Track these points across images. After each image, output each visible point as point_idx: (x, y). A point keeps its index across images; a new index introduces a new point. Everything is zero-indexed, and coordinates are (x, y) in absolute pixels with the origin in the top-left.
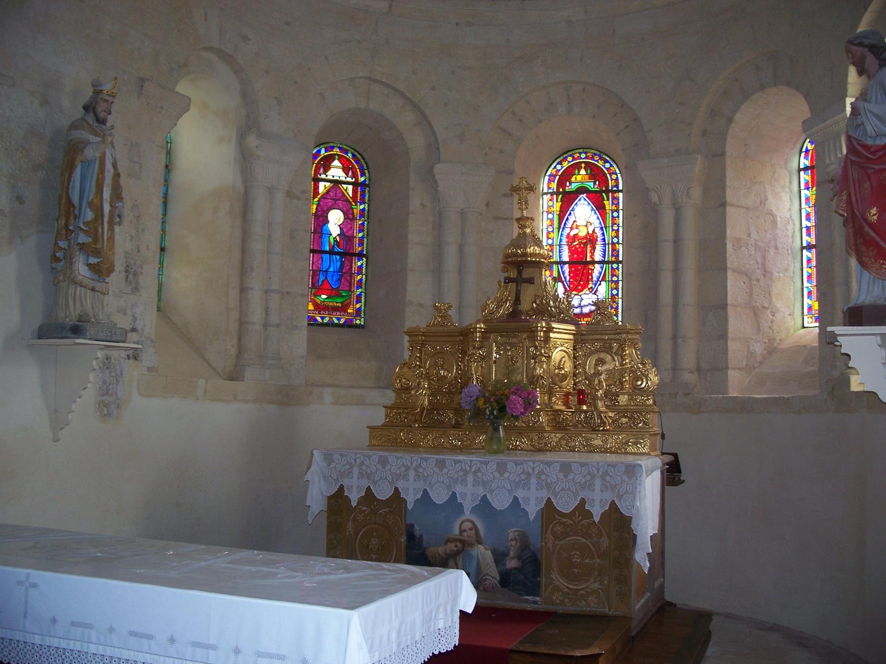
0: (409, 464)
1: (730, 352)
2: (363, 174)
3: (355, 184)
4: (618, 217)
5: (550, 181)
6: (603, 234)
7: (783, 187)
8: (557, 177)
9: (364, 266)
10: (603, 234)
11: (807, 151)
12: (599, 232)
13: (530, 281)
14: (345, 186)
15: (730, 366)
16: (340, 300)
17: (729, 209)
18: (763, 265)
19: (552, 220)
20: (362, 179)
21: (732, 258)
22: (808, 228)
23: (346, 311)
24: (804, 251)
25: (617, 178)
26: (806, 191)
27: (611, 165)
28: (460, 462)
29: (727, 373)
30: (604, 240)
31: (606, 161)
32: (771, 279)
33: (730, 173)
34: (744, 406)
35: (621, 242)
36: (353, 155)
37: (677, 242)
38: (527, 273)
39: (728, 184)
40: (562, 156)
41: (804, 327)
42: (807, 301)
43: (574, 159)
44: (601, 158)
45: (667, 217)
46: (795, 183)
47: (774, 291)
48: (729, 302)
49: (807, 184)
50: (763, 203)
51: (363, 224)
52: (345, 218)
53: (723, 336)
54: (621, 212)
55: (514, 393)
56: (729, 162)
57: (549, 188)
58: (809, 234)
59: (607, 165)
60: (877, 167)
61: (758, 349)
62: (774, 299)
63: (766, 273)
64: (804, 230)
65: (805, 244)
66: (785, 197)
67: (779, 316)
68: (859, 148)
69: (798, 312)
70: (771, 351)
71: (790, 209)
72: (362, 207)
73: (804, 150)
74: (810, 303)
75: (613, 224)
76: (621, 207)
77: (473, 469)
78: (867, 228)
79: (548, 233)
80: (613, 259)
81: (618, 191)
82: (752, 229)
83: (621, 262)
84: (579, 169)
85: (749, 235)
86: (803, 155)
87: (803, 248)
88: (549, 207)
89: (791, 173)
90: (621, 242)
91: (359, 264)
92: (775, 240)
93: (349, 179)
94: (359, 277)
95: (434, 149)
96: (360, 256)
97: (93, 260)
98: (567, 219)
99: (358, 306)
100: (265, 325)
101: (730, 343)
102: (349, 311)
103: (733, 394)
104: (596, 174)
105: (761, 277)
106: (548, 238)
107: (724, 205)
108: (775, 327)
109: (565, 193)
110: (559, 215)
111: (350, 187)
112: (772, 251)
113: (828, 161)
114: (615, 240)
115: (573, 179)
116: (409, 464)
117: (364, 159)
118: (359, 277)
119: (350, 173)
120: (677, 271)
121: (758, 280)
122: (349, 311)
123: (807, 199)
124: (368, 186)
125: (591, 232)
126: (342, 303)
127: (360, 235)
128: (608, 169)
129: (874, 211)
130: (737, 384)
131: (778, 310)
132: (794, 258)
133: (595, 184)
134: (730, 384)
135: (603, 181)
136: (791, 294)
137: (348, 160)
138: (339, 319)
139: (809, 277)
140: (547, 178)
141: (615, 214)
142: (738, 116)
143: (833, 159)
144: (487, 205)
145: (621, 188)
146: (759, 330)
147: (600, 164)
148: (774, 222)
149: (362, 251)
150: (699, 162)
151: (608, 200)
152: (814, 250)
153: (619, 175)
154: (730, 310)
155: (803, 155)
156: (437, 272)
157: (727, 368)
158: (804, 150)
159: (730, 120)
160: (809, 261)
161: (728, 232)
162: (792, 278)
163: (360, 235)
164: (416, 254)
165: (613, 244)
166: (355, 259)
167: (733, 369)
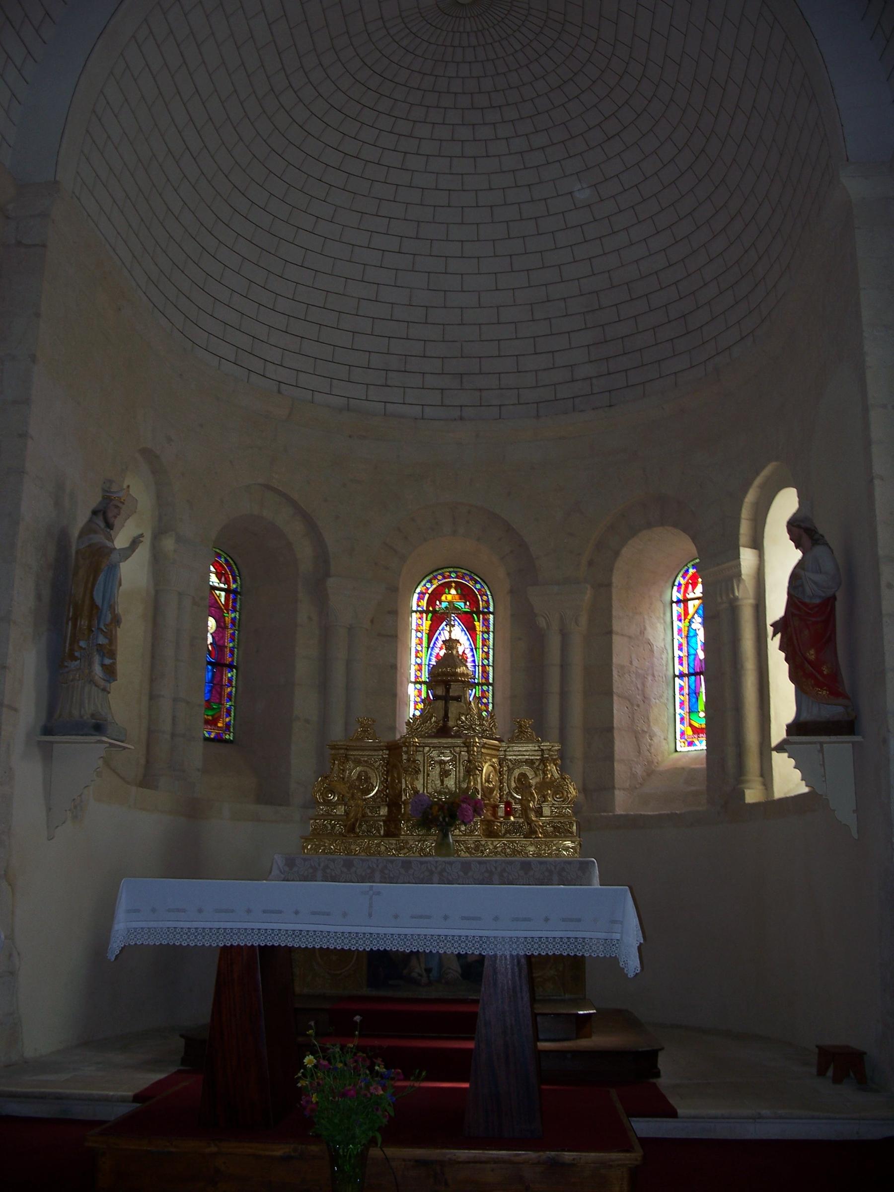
0: (375, 866)
1: (616, 773)
2: (235, 581)
3: (227, 591)
4: (488, 639)
5: (419, 599)
6: (473, 656)
7: (658, 618)
8: (427, 596)
9: (234, 678)
10: (473, 656)
11: (680, 585)
12: (469, 655)
13: (458, 699)
14: (217, 592)
15: (616, 786)
16: (210, 713)
17: (615, 637)
18: (643, 691)
19: (421, 639)
20: (234, 586)
21: (618, 684)
22: (680, 658)
23: (216, 724)
24: (676, 679)
25: (487, 600)
26: (679, 623)
27: (482, 586)
28: (426, 862)
29: (613, 793)
30: (474, 661)
31: (477, 582)
32: (649, 705)
33: (615, 604)
34: (632, 822)
35: (491, 664)
36: (226, 560)
37: (564, 666)
38: (454, 691)
39: (614, 613)
40: (431, 574)
41: (676, 751)
42: (679, 726)
43: (444, 578)
44: (472, 579)
45: (554, 642)
46: (669, 614)
47: (652, 717)
48: (615, 725)
49: (679, 616)
50: (642, 633)
51: (233, 634)
52: (217, 627)
53: (610, 757)
54: (491, 634)
55: (463, 802)
56: (614, 591)
57: (418, 606)
58: (681, 664)
59: (478, 586)
60: (814, 619)
61: (639, 770)
62: (652, 724)
63: (645, 699)
64: (677, 660)
65: (677, 673)
66: (660, 627)
67: (655, 740)
68: (799, 604)
69: (671, 737)
70: (650, 773)
71: (664, 639)
72: (233, 615)
73: (676, 583)
74: (683, 728)
75: (484, 645)
76: (491, 628)
77: (439, 869)
78: (807, 665)
79: (417, 651)
80: (484, 681)
81: (490, 613)
82: (634, 656)
83: (491, 684)
84: (450, 588)
85: (631, 663)
86: (675, 588)
87: (675, 676)
88: (418, 625)
89: (664, 606)
90: (491, 664)
91: (229, 675)
92: (653, 668)
93: (222, 585)
94: (229, 690)
95: (323, 559)
96: (231, 667)
97: (107, 661)
98: (437, 638)
99: (227, 720)
100: (173, 735)
101: (616, 764)
102: (220, 725)
103: (619, 811)
104: (466, 594)
105: (641, 704)
106: (417, 657)
107: (610, 632)
108: (653, 751)
109: (434, 612)
110: (428, 634)
111: (223, 594)
112: (650, 678)
113: (719, 600)
114: (486, 662)
115: (443, 598)
116: (375, 866)
117: (236, 564)
118: (229, 690)
119: (223, 579)
120: (564, 695)
121: (638, 706)
122: (220, 725)
123: (680, 630)
124: (239, 593)
125: (461, 653)
126: (212, 716)
127: (231, 645)
128: (479, 590)
129: (812, 652)
130: (622, 802)
131: (655, 735)
132: (668, 685)
133: (465, 604)
134: (617, 803)
135: (474, 602)
136: (665, 720)
137: (221, 565)
138: (210, 733)
139: (682, 703)
140: (416, 596)
141: (486, 636)
142: (624, 551)
143: (724, 598)
144: (372, 621)
145: (491, 609)
146: (639, 752)
147: (470, 584)
148: (652, 651)
149: (233, 661)
150: (588, 592)
151: (479, 621)
152: (686, 679)
153: (490, 597)
154: (616, 734)
155: (675, 588)
156: (324, 686)
157: (613, 788)
158: (676, 583)
159: (617, 554)
160: (681, 688)
161: (614, 660)
162: (666, 705)
163: (231, 645)
164: (304, 667)
165: (483, 666)
166: (225, 670)
167: (619, 789)
